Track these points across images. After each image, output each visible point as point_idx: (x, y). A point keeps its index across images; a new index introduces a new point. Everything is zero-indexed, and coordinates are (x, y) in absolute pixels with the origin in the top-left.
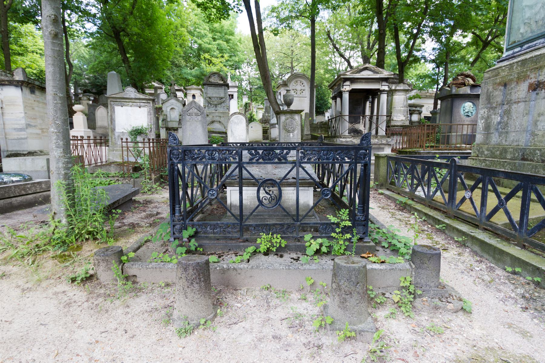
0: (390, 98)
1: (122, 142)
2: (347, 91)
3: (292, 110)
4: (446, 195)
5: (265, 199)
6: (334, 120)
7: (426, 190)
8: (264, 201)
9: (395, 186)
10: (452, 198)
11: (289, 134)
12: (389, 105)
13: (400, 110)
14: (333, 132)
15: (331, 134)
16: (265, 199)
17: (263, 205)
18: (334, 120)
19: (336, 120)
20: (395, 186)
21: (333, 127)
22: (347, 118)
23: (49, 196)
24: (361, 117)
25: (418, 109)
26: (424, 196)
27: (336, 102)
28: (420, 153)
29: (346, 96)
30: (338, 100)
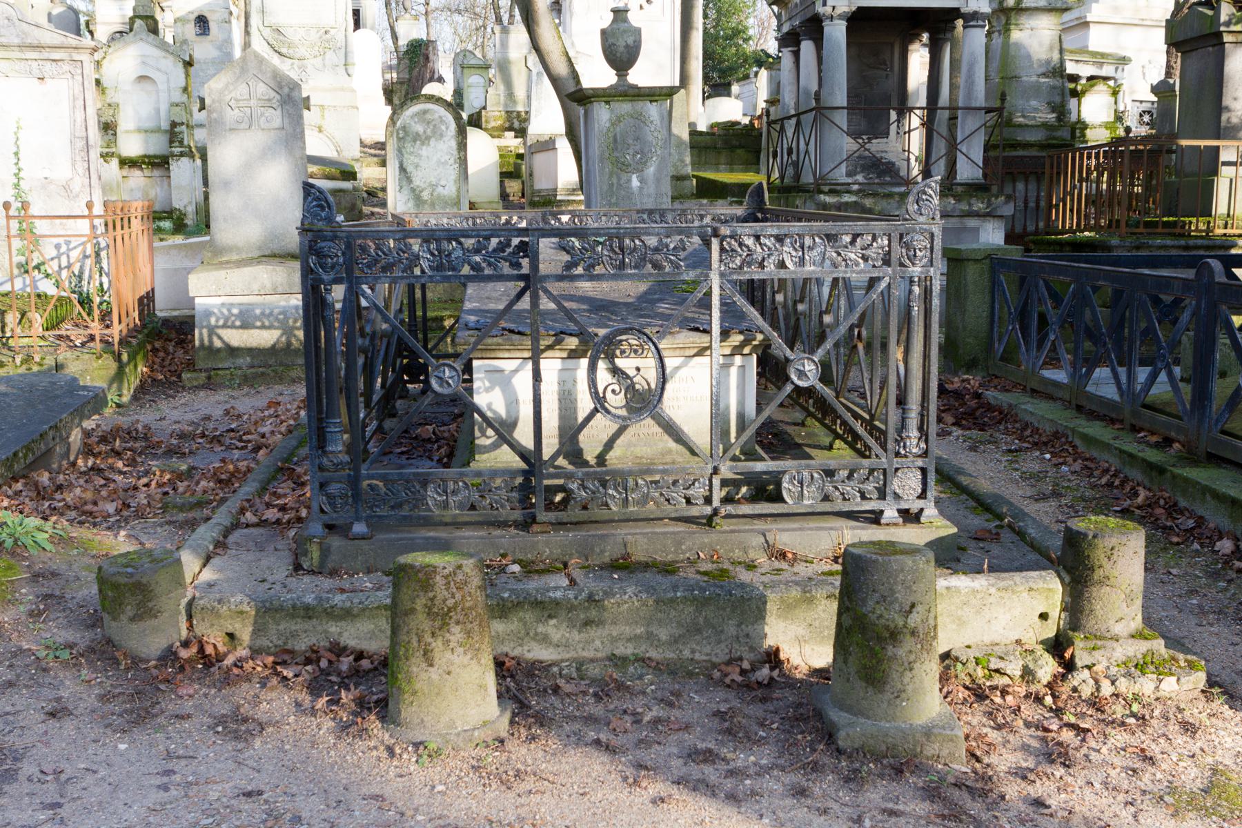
0: (997, 40)
1: (8, 217)
2: (840, 17)
3: (635, 87)
4: (1186, 389)
5: (613, 391)
6: (790, 126)
7: (1124, 378)
8: (609, 395)
9: (879, 279)
10: (1202, 396)
11: (624, 177)
12: (995, 65)
13: (1036, 88)
14: (790, 171)
15: (782, 177)
16: (613, 391)
17: (608, 412)
18: (790, 126)
19: (798, 124)
20: (879, 279)
21: (790, 152)
22: (842, 119)
23: (779, 280)
24: (893, 115)
25: (1107, 71)
26: (1117, 398)
27: (796, 54)
28: (1109, 248)
29: (837, 32)
30: (807, 47)
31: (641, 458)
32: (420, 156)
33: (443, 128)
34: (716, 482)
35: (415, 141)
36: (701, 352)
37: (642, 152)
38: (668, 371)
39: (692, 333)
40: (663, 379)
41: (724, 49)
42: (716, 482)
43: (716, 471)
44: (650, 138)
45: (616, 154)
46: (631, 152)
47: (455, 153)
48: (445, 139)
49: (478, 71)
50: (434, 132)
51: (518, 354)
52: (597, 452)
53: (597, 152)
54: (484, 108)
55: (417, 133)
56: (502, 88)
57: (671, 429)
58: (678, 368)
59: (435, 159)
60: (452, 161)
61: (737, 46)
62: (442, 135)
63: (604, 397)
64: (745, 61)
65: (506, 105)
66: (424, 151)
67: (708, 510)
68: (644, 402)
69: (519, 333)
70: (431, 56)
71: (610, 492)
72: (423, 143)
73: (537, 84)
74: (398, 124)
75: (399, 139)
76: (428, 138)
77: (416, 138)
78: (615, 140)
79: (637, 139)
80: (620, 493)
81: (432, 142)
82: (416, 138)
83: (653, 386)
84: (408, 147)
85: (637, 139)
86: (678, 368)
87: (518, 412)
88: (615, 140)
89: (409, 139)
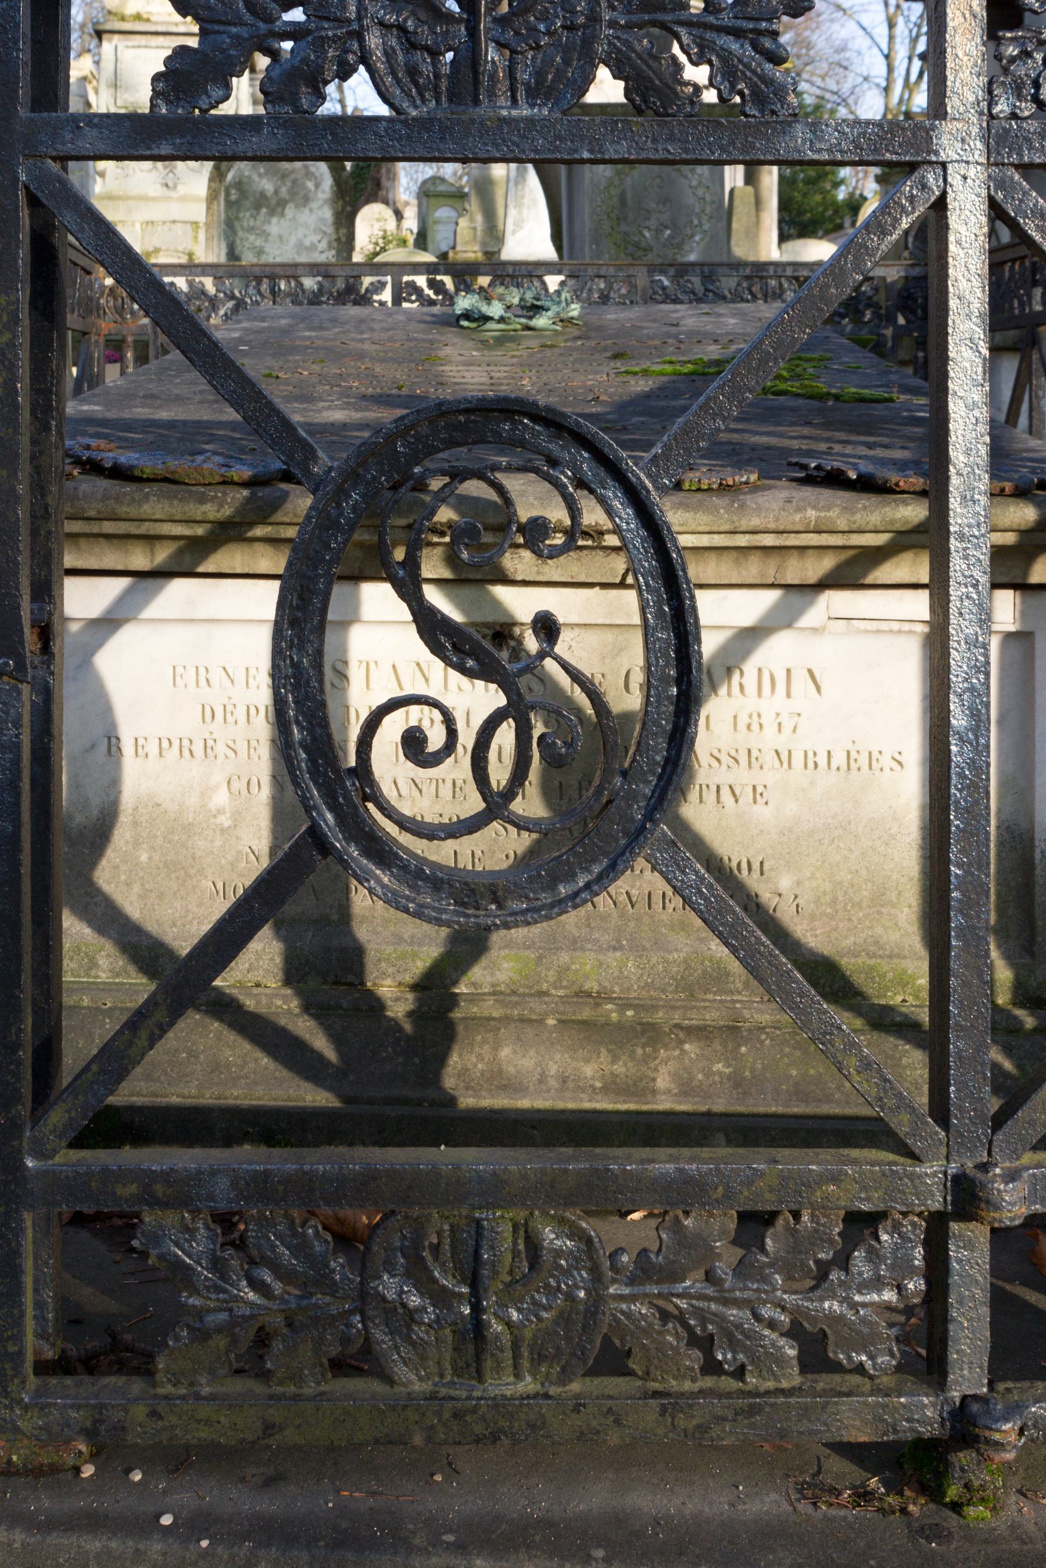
16: (413, 743)
31: (599, 998)
32: (266, 235)
33: (310, 185)
34: (970, 1254)
35: (257, 207)
36: (852, 572)
37: (674, 226)
38: (709, 644)
39: (809, 493)
40: (682, 674)
41: (805, 195)
42: (970, 1254)
43: (967, 1197)
44: (690, 200)
45: (624, 228)
46: (653, 223)
47: (330, 230)
48: (314, 205)
49: (451, 202)
50: (293, 193)
51: (110, 560)
52: (419, 966)
53: (588, 224)
54: (454, 248)
55: (263, 195)
56: (479, 218)
57: (727, 900)
58: (750, 637)
59: (293, 240)
60: (324, 244)
61: (824, 192)
62: (307, 199)
63: (363, 770)
64: (836, 211)
65: (484, 244)
66: (275, 227)
67: (923, 1412)
68: (615, 783)
69: (119, 473)
70: (384, 182)
71: (389, 1286)
72: (272, 213)
73: (517, 183)
74: (230, 177)
75: (229, 204)
76: (282, 204)
77: (261, 202)
78: (623, 202)
79: (665, 200)
80: (441, 1297)
81: (290, 211)
82: (261, 202)
83: (631, 701)
84: (246, 218)
85: (665, 200)
86: (750, 637)
87: (114, 783)
88: (623, 202)
89: (247, 203)
